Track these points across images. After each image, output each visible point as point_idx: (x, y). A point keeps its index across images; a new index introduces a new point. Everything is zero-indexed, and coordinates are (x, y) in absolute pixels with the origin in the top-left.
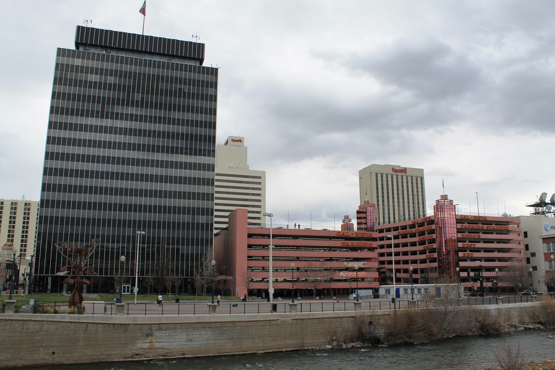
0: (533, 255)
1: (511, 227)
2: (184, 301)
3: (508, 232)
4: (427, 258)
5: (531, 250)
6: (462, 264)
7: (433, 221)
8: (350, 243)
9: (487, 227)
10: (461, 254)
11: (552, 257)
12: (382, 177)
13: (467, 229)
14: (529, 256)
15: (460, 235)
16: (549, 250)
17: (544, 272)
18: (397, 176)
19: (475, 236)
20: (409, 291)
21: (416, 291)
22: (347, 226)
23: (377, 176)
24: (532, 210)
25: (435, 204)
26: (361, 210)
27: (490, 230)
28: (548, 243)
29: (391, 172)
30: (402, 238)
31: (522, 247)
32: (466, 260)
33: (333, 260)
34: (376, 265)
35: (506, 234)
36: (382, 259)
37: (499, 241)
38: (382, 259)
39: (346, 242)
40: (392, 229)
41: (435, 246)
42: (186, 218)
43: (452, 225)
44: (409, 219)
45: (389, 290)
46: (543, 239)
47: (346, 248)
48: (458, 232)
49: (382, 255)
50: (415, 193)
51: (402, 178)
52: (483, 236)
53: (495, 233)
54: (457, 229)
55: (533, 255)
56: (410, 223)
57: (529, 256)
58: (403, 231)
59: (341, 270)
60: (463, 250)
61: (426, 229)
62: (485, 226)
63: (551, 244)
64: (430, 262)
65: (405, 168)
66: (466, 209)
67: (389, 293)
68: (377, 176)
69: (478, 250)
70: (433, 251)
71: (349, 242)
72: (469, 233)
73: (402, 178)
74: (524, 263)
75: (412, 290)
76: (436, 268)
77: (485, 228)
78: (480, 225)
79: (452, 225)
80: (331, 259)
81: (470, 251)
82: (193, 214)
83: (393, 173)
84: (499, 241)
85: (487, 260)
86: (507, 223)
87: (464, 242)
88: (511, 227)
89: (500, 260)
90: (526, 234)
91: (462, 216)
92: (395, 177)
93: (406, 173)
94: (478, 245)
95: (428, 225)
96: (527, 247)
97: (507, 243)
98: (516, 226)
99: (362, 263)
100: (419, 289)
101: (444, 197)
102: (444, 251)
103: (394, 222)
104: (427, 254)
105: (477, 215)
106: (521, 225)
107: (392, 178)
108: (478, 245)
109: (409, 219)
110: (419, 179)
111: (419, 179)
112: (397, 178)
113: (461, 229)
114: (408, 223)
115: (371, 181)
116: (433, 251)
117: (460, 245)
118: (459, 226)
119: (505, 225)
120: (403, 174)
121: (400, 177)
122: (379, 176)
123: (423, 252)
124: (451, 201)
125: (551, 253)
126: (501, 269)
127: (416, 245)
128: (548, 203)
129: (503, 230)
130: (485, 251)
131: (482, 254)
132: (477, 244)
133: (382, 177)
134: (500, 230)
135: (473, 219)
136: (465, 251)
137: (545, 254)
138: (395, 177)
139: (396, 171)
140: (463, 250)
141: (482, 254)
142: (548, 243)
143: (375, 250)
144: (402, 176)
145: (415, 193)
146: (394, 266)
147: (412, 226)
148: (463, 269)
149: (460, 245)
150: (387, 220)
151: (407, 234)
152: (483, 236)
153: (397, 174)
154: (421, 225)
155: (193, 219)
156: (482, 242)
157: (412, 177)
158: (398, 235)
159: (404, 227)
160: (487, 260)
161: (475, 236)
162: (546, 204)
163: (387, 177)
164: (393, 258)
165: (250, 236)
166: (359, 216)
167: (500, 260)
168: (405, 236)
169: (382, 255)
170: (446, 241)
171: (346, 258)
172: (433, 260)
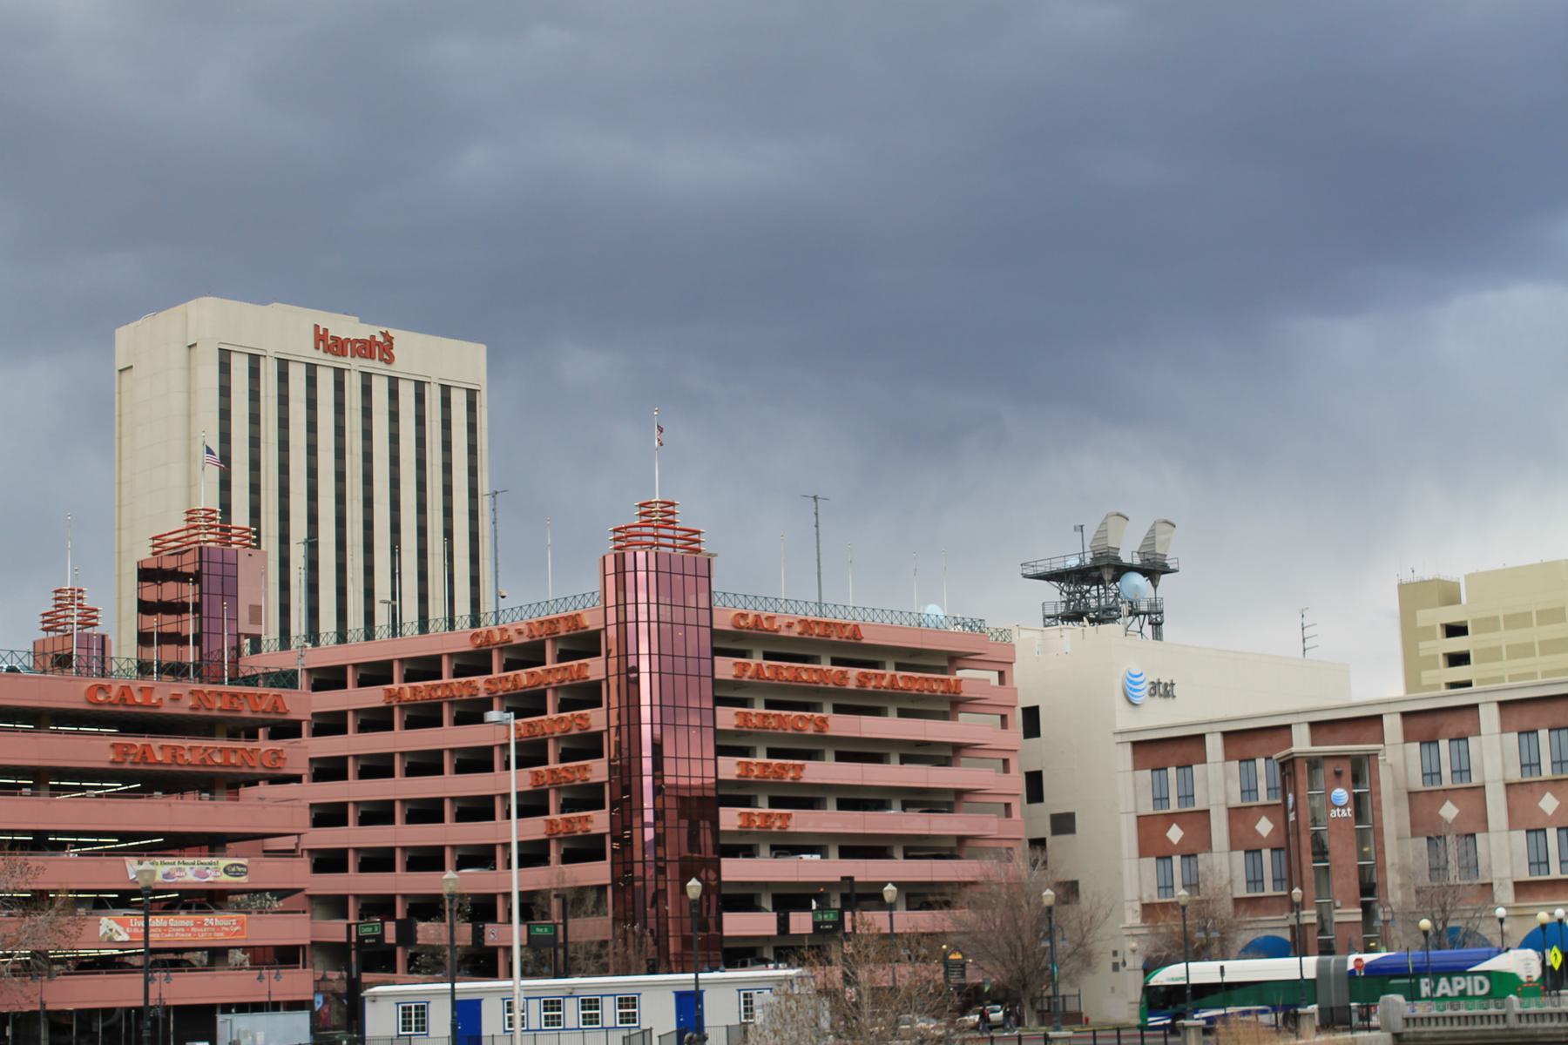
0: (1064, 823)
3: (954, 704)
4: (552, 835)
5: (1056, 799)
6: (734, 870)
7: (595, 636)
8: (159, 750)
10: (730, 818)
11: (1549, 803)
12: (254, 373)
14: (1044, 830)
16: (1161, 799)
17: (1133, 918)
18: (339, 374)
20: (609, 1012)
21: (572, 1013)
23: (225, 368)
24: (1052, 594)
26: (169, 564)
27: (875, 694)
28: (1159, 768)
30: (410, 724)
31: (1018, 784)
32: (749, 851)
33: (61, 847)
35: (944, 716)
36: (330, 838)
37: (915, 752)
38: (330, 838)
39: (139, 741)
40: (351, 676)
45: (422, 1011)
46: (1135, 744)
47: (125, 777)
49: (330, 815)
51: (367, 391)
55: (1064, 823)
56: (462, 641)
57: (1044, 830)
58: (430, 689)
59: (99, 903)
61: (553, 680)
62: (853, 673)
63: (1172, 771)
64: (569, 857)
67: (422, 1026)
68: (225, 368)
69: (809, 799)
71: (156, 743)
73: (367, 391)
74: (1020, 865)
75: (590, 1004)
76: (601, 889)
77: (852, 685)
80: (41, 842)
81: (774, 802)
83: (319, 357)
84: (915, 752)
85: (855, 848)
86: (954, 659)
89: (917, 848)
90: (1032, 721)
92: (325, 381)
93: (390, 361)
95: (563, 656)
96: (1035, 785)
97: (945, 762)
98: (993, 677)
99: (224, 862)
100: (590, 1004)
103: (342, 637)
104: (554, 815)
106: (1018, 674)
107: (312, 382)
112: (339, 386)
113: (735, 684)
115: (190, 392)
119: (942, 670)
120: (374, 365)
122: (240, 368)
125: (1171, 818)
126: (918, 896)
128: (1131, 568)
130: (844, 805)
131: (830, 820)
133: (254, 373)
134: (918, 698)
135: (795, 632)
137: (1142, 820)
138: (325, 381)
140: (737, 795)
141: (830, 820)
142: (1159, 768)
143: (245, 792)
144: (367, 378)
146: (515, 880)
147: (473, 663)
148: (744, 899)
151: (439, 707)
153: (341, 362)
154: (528, 655)
156: (830, 755)
157: (420, 387)
159: (424, 668)
160: (855, 848)
162: (1121, 570)
163: (283, 377)
164: (514, 830)
167: (917, 848)
168: (424, 716)
169: (330, 815)
171: (124, 836)
172: (583, 850)
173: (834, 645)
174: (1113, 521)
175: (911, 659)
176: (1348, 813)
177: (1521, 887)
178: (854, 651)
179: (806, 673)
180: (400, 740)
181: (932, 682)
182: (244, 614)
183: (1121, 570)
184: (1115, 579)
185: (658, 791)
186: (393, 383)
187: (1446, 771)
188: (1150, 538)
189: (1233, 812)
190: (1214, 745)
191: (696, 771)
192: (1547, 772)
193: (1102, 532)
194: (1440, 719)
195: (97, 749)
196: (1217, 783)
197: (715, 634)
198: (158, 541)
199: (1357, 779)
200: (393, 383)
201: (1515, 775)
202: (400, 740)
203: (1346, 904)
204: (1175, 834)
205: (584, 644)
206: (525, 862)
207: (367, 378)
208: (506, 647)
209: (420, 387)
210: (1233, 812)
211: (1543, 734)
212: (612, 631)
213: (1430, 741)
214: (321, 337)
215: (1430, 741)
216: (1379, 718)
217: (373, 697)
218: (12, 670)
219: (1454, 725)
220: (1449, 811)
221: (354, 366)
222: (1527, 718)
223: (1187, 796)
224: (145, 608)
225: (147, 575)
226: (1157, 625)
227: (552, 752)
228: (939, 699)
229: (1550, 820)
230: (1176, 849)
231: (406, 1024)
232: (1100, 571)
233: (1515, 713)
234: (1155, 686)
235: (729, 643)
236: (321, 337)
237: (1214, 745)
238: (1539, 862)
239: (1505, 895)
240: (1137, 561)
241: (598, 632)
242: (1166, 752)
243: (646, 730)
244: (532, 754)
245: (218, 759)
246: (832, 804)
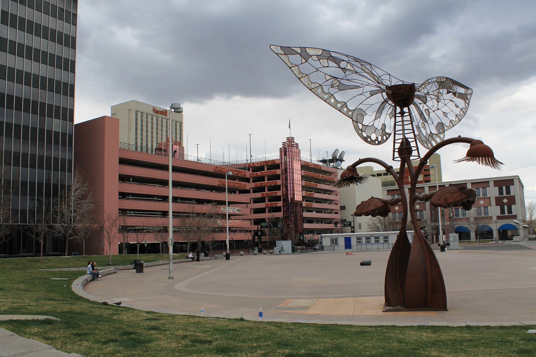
2: (329, 252)
4: (266, 207)
23: (137, 115)
25: (281, 146)
29: (151, 112)
34: (246, 211)
41: (279, 193)
42: (31, 120)
45: (336, 240)
51: (162, 121)
65: (166, 110)
67: (336, 243)
68: (137, 115)
73: (162, 121)
82: (42, 115)
91: (305, 162)
92: (155, 118)
93: (166, 115)
99: (237, 208)
101: (290, 140)
105: (309, 161)
110: (178, 124)
111: (178, 124)
116: (278, 199)
121: (160, 119)
122: (139, 114)
138: (155, 118)
151: (264, 177)
155: (42, 123)
165: (123, 161)
190: (492, 184)
208: (267, 165)
211: (481, 189)
212: (283, 164)
220: (505, 201)
227: (266, 189)
231: (332, 243)
237: (492, 184)
241: (279, 164)
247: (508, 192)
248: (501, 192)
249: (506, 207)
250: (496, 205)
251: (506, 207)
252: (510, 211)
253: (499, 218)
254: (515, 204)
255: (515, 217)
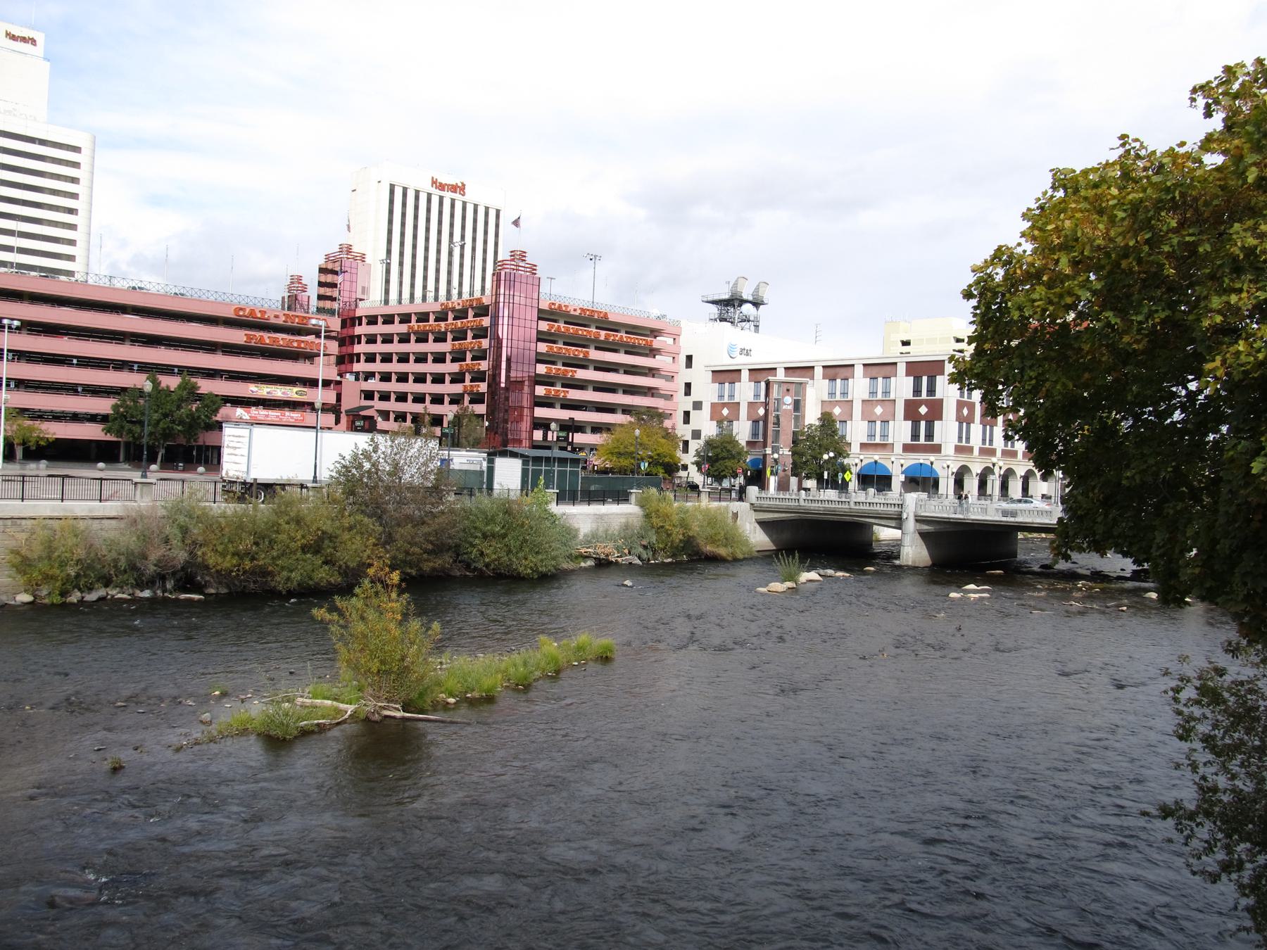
1: (657, 343)
3: (653, 352)
4: (465, 392)
9: (607, 336)
10: (540, 391)
13: (596, 340)
14: (689, 408)
15: (543, 347)
16: (721, 396)
18: (441, 199)
19: (579, 353)
22: (293, 301)
24: (714, 309)
26: (330, 266)
27: (613, 343)
35: (646, 355)
37: (631, 370)
41: (484, 365)
43: (522, 324)
44: (436, 298)
48: (539, 340)
50: (457, 237)
52: (595, 355)
53: (622, 351)
54: (539, 332)
55: (698, 405)
56: (438, 308)
57: (689, 408)
60: (546, 381)
62: (603, 333)
66: (571, 289)
69: (581, 385)
70: (478, 377)
72: (565, 344)
73: (453, 206)
77: (602, 338)
78: (562, 325)
79: (528, 324)
83: (436, 194)
84: (631, 370)
86: (655, 333)
87: (553, 363)
88: (657, 343)
94: (581, 374)
98: (670, 341)
99: (295, 389)
102: (503, 379)
107: (429, 201)
108: (581, 374)
109: (436, 298)
113: (549, 333)
114: (432, 306)
116: (478, 377)
117: (542, 369)
118: (544, 326)
120: (457, 196)
123: (457, 378)
124: (533, 268)
125: (724, 405)
127: (444, 361)
129: (639, 346)
130: (596, 389)
132: (579, 371)
134: (634, 346)
136: (552, 385)
139: (442, 187)
140: (546, 381)
144: (453, 201)
145: (457, 237)
147: (442, 317)
149: (542, 369)
150: (406, 295)
152: (595, 355)
153: (442, 193)
154: (461, 314)
156: (591, 367)
157: (476, 206)
158: (409, 334)
159: (423, 317)
161: (579, 353)
162: (743, 302)
166: (323, 280)
170: (509, 360)
173: (597, 321)
174: (741, 281)
175: (633, 330)
176: (791, 407)
177: (863, 446)
178: (605, 324)
179: (581, 331)
180: (413, 347)
181: (640, 341)
182: (359, 290)
183: (743, 302)
184: (740, 306)
185: (508, 377)
186: (464, 204)
187: (838, 393)
188: (757, 289)
189: (750, 404)
191: (526, 369)
192: (880, 396)
193: (736, 284)
194: (838, 370)
195: (237, 336)
196: (745, 391)
197: (540, 311)
198: (327, 257)
199: (797, 394)
200: (464, 204)
201: (866, 397)
202: (413, 347)
203: (785, 446)
204: (879, 410)
205: (482, 311)
206: (397, 400)
207: (453, 201)
209: (476, 206)
210: (750, 404)
211: (880, 380)
213: (833, 379)
214: (434, 182)
215: (833, 379)
216: (813, 367)
217: (403, 328)
218: (134, 288)
219: (843, 372)
221: (448, 196)
222: (875, 370)
223: (731, 396)
224: (321, 284)
225: (322, 271)
226: (757, 326)
228: (644, 348)
229: (878, 417)
230: (726, 418)
232: (733, 302)
233: (870, 368)
234: (742, 350)
235: (543, 315)
236: (434, 182)
238: (872, 436)
239: (898, 449)
240: (750, 298)
242: (726, 376)
243: (504, 350)
244: (458, 357)
245: (295, 344)
246: (591, 388)
247: (931, 391)
248: (917, 391)
249: (923, 424)
250: (906, 418)
251: (923, 424)
252: (930, 436)
253: (907, 448)
254: (941, 419)
255: (937, 449)
